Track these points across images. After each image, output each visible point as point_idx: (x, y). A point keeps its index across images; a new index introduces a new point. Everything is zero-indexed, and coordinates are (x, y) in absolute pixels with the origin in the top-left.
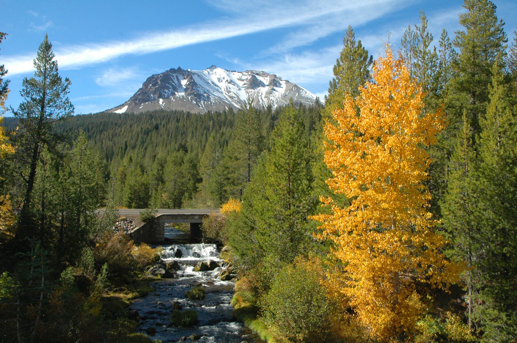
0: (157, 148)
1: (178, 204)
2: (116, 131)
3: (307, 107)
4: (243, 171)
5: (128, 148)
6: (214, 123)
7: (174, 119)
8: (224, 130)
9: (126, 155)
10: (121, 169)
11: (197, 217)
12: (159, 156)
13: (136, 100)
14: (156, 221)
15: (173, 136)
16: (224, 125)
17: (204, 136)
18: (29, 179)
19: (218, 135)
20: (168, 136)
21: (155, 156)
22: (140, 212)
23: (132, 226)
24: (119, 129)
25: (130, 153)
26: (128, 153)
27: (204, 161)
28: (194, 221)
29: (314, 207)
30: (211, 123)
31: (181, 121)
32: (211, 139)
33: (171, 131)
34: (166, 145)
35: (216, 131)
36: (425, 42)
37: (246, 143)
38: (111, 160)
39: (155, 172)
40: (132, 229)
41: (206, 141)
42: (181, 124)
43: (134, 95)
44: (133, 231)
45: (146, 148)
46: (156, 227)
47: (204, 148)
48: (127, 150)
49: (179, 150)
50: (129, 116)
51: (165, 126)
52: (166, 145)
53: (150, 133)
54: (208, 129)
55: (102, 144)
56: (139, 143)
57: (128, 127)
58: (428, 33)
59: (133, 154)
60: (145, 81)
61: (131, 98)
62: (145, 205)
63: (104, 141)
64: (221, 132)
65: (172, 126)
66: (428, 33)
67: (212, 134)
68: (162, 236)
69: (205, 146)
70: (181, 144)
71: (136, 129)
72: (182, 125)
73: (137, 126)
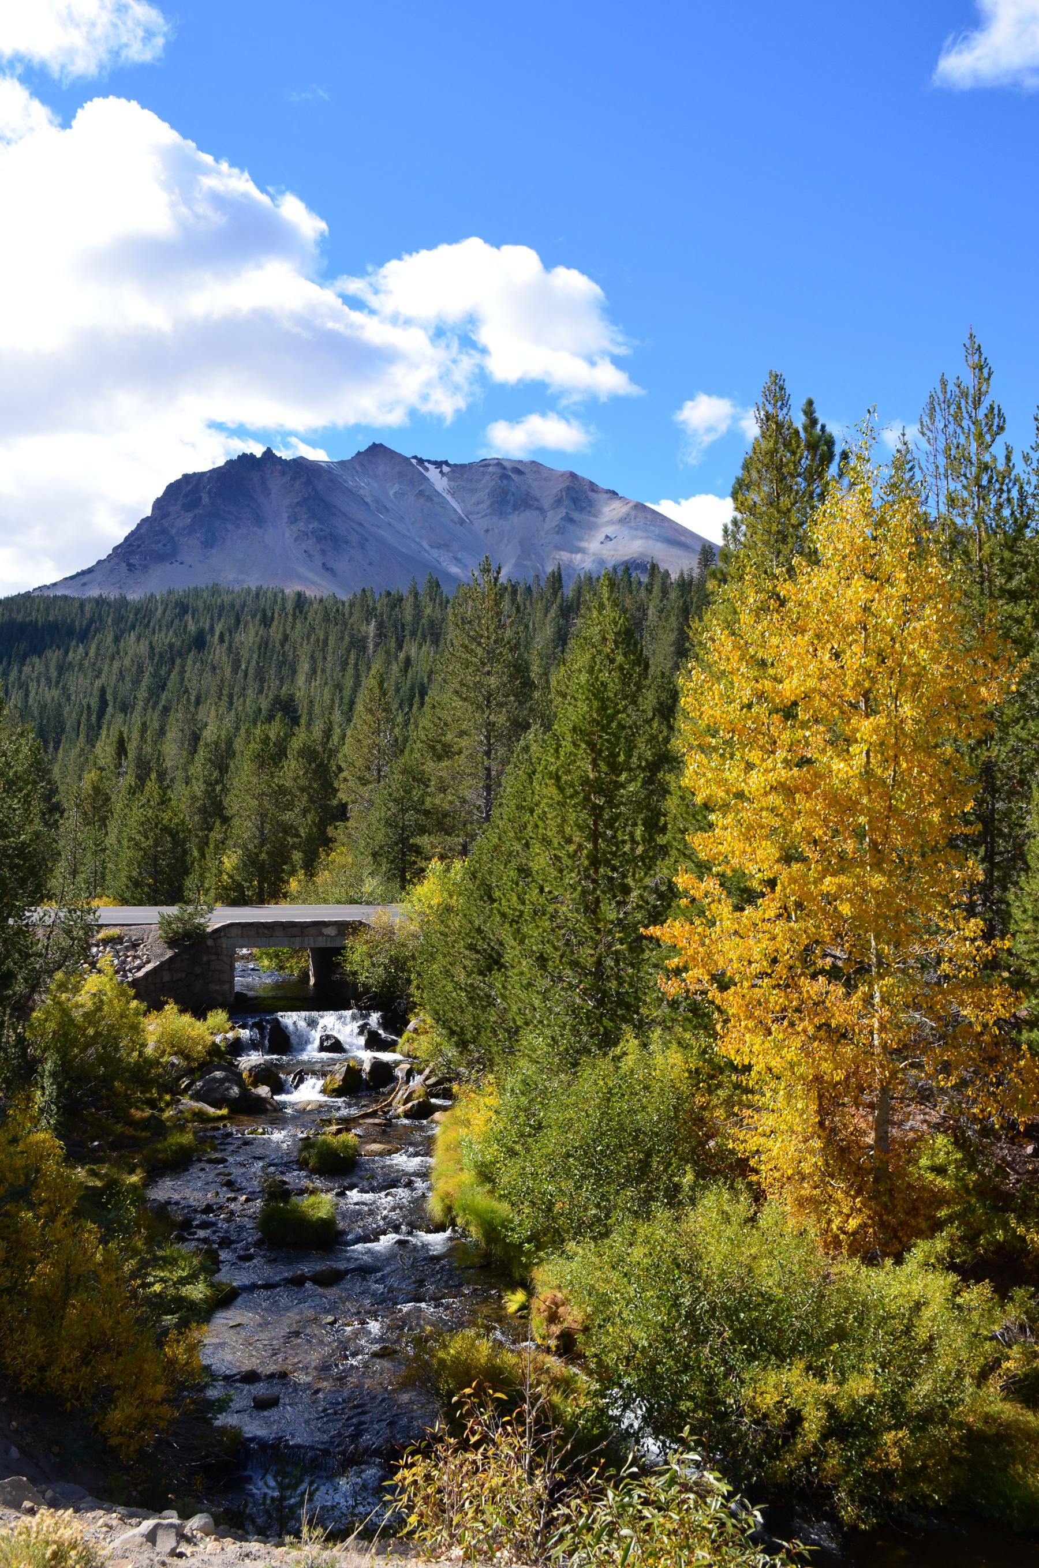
0: (203, 709)
1: (271, 891)
2: (71, 655)
3: (674, 576)
4: (471, 790)
5: (110, 710)
6: (380, 625)
7: (254, 617)
8: (413, 651)
9: (104, 732)
10: (91, 776)
11: (330, 931)
12: (209, 734)
13: (132, 553)
14: (210, 942)
15: (251, 671)
16: (413, 634)
17: (350, 670)
18: (1027, 1283)
19: (395, 668)
20: (235, 669)
21: (196, 738)
22: (163, 917)
23: (135, 957)
24: (81, 649)
25: (115, 725)
26: (110, 723)
27: (351, 752)
28: (321, 943)
29: (665, 902)
30: (372, 629)
31: (275, 623)
32: (370, 682)
33: (244, 653)
34: (231, 697)
35: (388, 652)
36: (981, 435)
37: (479, 707)
38: (56, 749)
39: (198, 788)
40: (139, 968)
41: (357, 684)
42: (275, 633)
43: (126, 539)
44: (140, 974)
45: (166, 710)
46: (209, 962)
47: (351, 709)
48: (107, 716)
49: (270, 718)
50: (109, 605)
51: (227, 638)
52: (231, 697)
53: (178, 661)
54: (364, 649)
55: (27, 695)
56: (142, 694)
57: (110, 639)
58: (992, 408)
59: (128, 726)
60: (160, 494)
61: (115, 549)
62: (174, 896)
63: (33, 687)
64: (402, 656)
65: (248, 637)
66: (992, 408)
67: (376, 667)
68: (226, 987)
69: (352, 703)
70: (277, 697)
71: (135, 646)
72: (280, 636)
73: (138, 639)
